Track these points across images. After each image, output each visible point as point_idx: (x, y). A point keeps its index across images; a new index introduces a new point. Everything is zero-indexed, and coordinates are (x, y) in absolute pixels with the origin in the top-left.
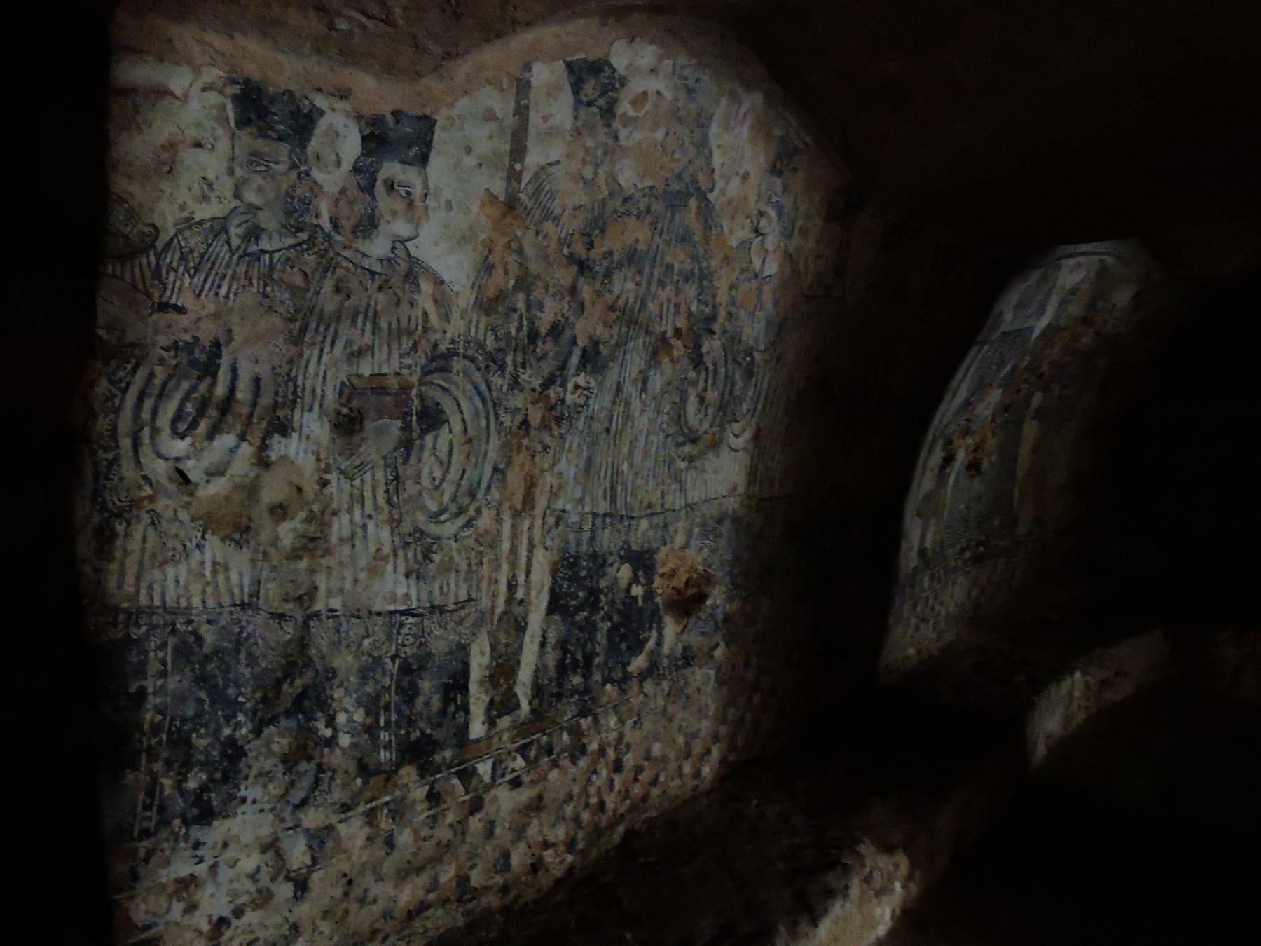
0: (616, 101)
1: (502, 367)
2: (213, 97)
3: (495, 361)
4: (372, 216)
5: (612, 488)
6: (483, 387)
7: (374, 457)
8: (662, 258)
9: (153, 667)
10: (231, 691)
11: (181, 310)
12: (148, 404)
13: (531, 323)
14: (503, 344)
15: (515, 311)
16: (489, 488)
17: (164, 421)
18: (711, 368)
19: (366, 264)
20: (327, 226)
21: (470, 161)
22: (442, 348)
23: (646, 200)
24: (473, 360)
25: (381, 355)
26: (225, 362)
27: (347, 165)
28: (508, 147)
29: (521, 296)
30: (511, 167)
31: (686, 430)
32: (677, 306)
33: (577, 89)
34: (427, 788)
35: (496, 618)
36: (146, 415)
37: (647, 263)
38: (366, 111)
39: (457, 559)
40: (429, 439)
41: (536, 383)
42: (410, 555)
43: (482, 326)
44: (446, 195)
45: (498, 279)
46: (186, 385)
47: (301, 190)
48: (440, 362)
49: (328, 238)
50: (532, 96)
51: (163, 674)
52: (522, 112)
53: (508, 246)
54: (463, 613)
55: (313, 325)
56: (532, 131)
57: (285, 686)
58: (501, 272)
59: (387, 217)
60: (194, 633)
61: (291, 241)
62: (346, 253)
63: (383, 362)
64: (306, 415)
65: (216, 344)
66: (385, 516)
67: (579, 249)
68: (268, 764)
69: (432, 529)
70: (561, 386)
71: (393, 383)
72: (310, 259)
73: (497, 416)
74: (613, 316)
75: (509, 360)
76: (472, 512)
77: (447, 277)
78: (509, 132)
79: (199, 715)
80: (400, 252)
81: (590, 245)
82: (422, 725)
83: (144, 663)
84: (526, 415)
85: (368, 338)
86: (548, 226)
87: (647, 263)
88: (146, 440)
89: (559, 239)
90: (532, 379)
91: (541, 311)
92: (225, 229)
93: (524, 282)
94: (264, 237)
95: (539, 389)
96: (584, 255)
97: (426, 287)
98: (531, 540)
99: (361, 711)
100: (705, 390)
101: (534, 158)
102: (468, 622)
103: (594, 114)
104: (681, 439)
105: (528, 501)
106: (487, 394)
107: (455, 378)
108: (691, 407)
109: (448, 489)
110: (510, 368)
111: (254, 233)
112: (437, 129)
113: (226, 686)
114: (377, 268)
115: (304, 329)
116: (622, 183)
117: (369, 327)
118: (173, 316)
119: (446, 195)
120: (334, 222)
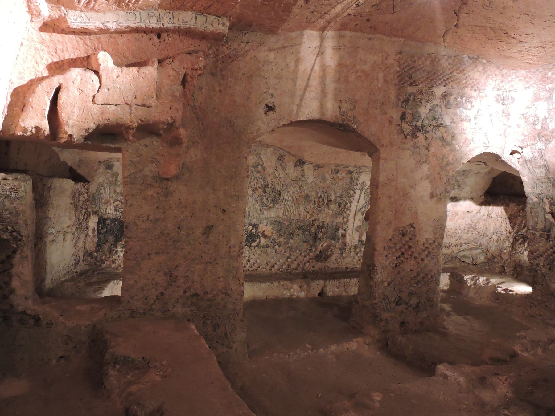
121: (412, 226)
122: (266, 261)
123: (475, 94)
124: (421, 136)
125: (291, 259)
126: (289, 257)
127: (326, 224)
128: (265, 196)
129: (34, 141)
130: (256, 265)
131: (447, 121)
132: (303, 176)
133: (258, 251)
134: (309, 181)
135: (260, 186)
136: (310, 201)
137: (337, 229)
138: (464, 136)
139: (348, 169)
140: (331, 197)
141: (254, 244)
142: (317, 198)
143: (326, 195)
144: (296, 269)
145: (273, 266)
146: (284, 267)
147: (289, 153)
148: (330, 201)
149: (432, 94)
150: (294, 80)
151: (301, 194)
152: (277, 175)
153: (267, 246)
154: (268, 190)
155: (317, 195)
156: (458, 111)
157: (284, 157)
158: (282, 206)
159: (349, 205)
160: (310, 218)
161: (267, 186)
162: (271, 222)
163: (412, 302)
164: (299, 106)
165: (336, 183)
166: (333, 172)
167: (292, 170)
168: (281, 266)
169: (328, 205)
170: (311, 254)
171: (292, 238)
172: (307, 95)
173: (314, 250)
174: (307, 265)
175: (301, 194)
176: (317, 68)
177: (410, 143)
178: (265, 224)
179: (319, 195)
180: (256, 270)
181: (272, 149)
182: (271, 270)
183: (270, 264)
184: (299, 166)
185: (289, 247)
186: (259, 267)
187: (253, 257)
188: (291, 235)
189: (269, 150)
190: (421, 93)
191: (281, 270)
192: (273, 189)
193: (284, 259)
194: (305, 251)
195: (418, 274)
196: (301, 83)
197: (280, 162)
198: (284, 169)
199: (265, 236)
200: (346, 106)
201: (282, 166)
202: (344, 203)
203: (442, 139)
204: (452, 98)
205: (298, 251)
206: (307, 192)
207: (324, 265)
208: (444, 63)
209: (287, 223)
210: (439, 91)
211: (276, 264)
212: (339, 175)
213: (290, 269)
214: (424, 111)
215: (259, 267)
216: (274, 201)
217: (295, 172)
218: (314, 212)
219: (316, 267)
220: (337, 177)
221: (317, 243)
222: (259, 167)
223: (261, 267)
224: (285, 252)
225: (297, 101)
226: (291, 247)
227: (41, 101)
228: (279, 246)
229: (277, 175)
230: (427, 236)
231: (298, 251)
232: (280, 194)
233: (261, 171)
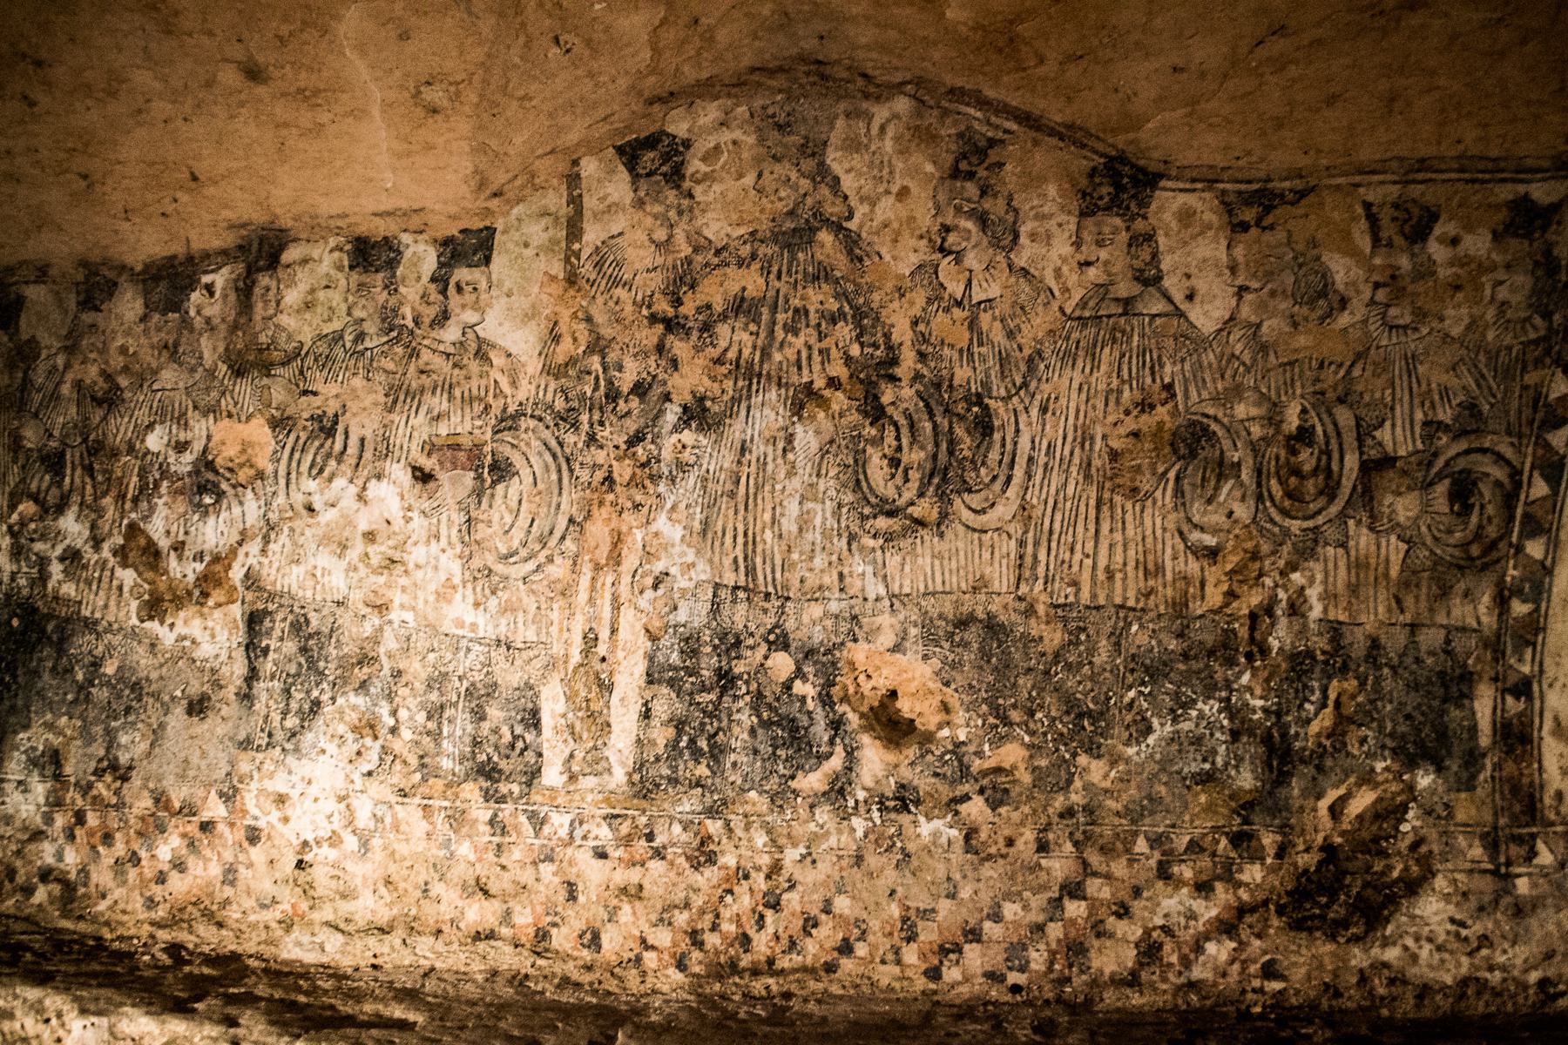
0: (682, 163)
1: (575, 426)
2: (336, 254)
3: (568, 419)
4: (445, 311)
5: (746, 558)
6: (553, 443)
7: (450, 501)
8: (787, 301)
9: (277, 633)
10: (322, 664)
11: (315, 394)
12: (297, 455)
13: (610, 382)
14: (575, 404)
15: (589, 373)
16: (563, 538)
17: (305, 467)
18: (903, 421)
19: (441, 348)
20: (411, 325)
21: (529, 252)
22: (511, 410)
23: (748, 247)
24: (540, 419)
25: (456, 419)
26: (340, 428)
27: (425, 279)
28: (564, 233)
29: (596, 359)
30: (568, 248)
31: (873, 500)
32: (824, 353)
33: (631, 167)
34: (491, 812)
35: (571, 668)
36: (294, 464)
37: (765, 311)
38: (440, 235)
39: (525, 600)
40: (500, 488)
41: (621, 440)
42: (479, 589)
43: (551, 390)
44: (508, 284)
45: (565, 349)
46: (317, 443)
47: (392, 302)
48: (508, 422)
49: (412, 333)
50: (584, 184)
51: (282, 639)
52: (576, 202)
53: (575, 315)
54: (531, 653)
55: (402, 397)
56: (587, 214)
57: (356, 670)
58: (570, 340)
59: (457, 311)
60: (304, 615)
61: (385, 339)
62: (425, 342)
63: (461, 424)
64: (395, 465)
65: (336, 415)
66: (458, 550)
67: (663, 306)
68: (341, 729)
69: (499, 568)
70: (653, 442)
71: (466, 442)
72: (399, 350)
73: (571, 471)
74: (724, 370)
75: (585, 418)
76: (542, 558)
77: (513, 351)
78: (563, 220)
79: (298, 675)
80: (470, 335)
81: (677, 302)
82: (490, 750)
83: (272, 629)
84: (610, 472)
85: (445, 405)
86: (619, 292)
87: (765, 311)
88: (293, 480)
89: (634, 303)
90: (611, 434)
91: (620, 371)
92: (342, 337)
93: (598, 346)
94: (367, 338)
95: (624, 447)
96: (670, 312)
97: (498, 360)
98: (615, 598)
99: (424, 714)
100: (899, 449)
101: (593, 235)
102: (538, 664)
103: (658, 183)
104: (867, 511)
105: (615, 559)
106: (558, 450)
107: (523, 436)
108: (877, 469)
109: (517, 535)
110: (586, 427)
111: (360, 337)
112: (498, 236)
113: (319, 660)
114: (451, 350)
115: (395, 402)
116: (710, 236)
117: (445, 396)
118: (311, 398)
119: (508, 284)
120: (417, 322)
122: (895, 910)
125: (724, 937)
126: (1073, 890)
127: (1357, 642)
128: (878, 441)
130: (827, 934)
132: (1149, 279)
133: (841, 836)
134: (1206, 317)
135: (838, 369)
136: (1224, 469)
137: (1455, 684)
139: (1505, 193)
140: (1384, 434)
141: (813, 781)
142: (1277, 450)
143: (1344, 416)
144: (1132, 980)
145: (949, 949)
146: (1037, 959)
147: (1028, 120)
148: (1376, 466)
151: (1146, 422)
152: (956, 288)
153: (904, 800)
154: (900, 396)
155: (1273, 418)
157: (993, 156)
158: (1004, 510)
159: (1540, 489)
160: (1231, 595)
162: (927, 624)
165: (1421, 315)
166: (1388, 230)
167: (1058, 250)
168: (1016, 953)
169: (1366, 495)
170: (1253, 873)
171: (1093, 750)
173: (1269, 840)
174: (1219, 951)
175: (1146, 422)
178: (887, 639)
179: (1292, 421)
180: (830, 968)
181: (902, 104)
182: (934, 974)
183: (928, 934)
184: (1115, 205)
185: (1068, 813)
186: (846, 948)
187: (807, 876)
188: (1086, 726)
189: (881, 113)
191: (1014, 978)
192: (935, 392)
193: (1038, 901)
194: (1194, 847)
197: (971, 189)
198: (1003, 236)
199: (891, 724)
201: (983, 220)
202: (1499, 473)
205: (1141, 846)
206: (1197, 400)
207: (1358, 958)
209: (1053, 637)
211: (974, 935)
212: (1436, 250)
213: (1079, 980)
215: (846, 948)
216: (945, 479)
217: (1089, 251)
218: (1255, 556)
219: (1298, 974)
220: (1425, 271)
221: (1296, 786)
222: (825, 237)
223: (861, 950)
224: (1043, 847)
226: (1089, 810)
228: (994, 805)
229: (956, 288)
231: (1141, 846)
232: (984, 427)
233: (841, 264)
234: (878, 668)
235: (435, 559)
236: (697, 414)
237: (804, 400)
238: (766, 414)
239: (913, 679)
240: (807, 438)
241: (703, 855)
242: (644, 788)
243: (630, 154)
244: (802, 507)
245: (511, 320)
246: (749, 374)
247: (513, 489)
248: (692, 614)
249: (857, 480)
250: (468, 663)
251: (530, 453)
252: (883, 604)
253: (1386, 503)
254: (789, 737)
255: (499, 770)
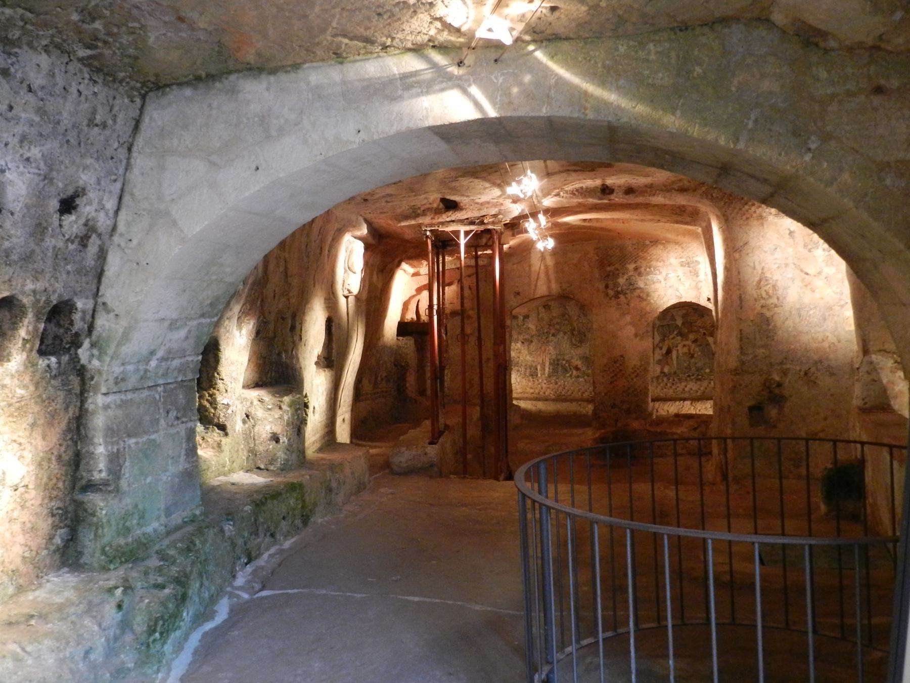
63: (527, 337)
121: (622, 356)
123: (659, 264)
124: (622, 297)
129: (411, 323)
131: (641, 284)
138: (657, 294)
149: (627, 269)
150: (529, 277)
153: (578, 377)
154: (576, 333)
156: (649, 277)
161: (574, 329)
163: (624, 407)
164: (535, 290)
172: (539, 284)
176: (542, 268)
177: (614, 302)
190: (617, 270)
192: (579, 332)
195: (629, 388)
196: (534, 277)
199: (577, 368)
200: (565, 286)
203: (639, 297)
204: (642, 270)
208: (630, 248)
210: (631, 267)
214: (621, 281)
216: (581, 342)
225: (533, 287)
227: (412, 307)
230: (634, 362)
234: (700, 345)
235: (525, 352)
236: (553, 335)
237: (565, 333)
238: (561, 334)
239: (579, 363)
240: (566, 338)
241: (556, 383)
242: (549, 376)
243: (544, 307)
244: (566, 345)
245: (532, 325)
246: (559, 331)
247: (534, 344)
248: (554, 357)
249: (571, 341)
250: (529, 363)
251: (535, 340)
252: (575, 355)
253: (630, 331)
254: (565, 370)
255: (534, 375)
